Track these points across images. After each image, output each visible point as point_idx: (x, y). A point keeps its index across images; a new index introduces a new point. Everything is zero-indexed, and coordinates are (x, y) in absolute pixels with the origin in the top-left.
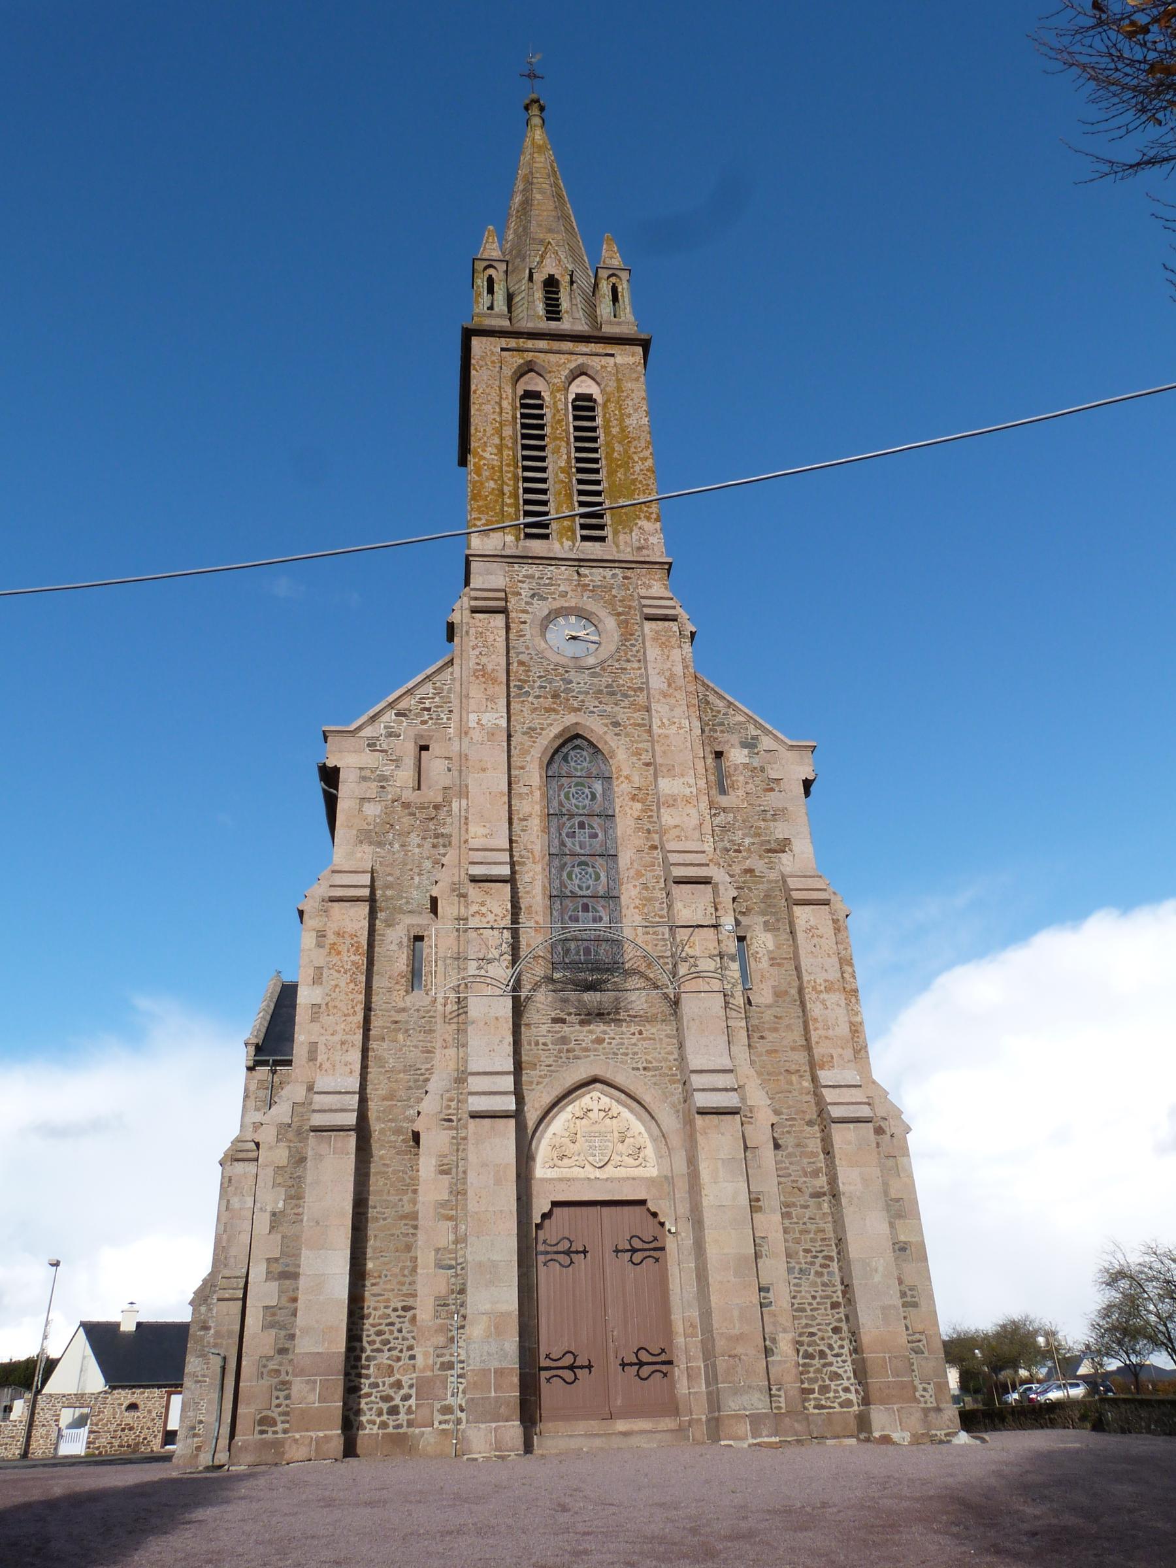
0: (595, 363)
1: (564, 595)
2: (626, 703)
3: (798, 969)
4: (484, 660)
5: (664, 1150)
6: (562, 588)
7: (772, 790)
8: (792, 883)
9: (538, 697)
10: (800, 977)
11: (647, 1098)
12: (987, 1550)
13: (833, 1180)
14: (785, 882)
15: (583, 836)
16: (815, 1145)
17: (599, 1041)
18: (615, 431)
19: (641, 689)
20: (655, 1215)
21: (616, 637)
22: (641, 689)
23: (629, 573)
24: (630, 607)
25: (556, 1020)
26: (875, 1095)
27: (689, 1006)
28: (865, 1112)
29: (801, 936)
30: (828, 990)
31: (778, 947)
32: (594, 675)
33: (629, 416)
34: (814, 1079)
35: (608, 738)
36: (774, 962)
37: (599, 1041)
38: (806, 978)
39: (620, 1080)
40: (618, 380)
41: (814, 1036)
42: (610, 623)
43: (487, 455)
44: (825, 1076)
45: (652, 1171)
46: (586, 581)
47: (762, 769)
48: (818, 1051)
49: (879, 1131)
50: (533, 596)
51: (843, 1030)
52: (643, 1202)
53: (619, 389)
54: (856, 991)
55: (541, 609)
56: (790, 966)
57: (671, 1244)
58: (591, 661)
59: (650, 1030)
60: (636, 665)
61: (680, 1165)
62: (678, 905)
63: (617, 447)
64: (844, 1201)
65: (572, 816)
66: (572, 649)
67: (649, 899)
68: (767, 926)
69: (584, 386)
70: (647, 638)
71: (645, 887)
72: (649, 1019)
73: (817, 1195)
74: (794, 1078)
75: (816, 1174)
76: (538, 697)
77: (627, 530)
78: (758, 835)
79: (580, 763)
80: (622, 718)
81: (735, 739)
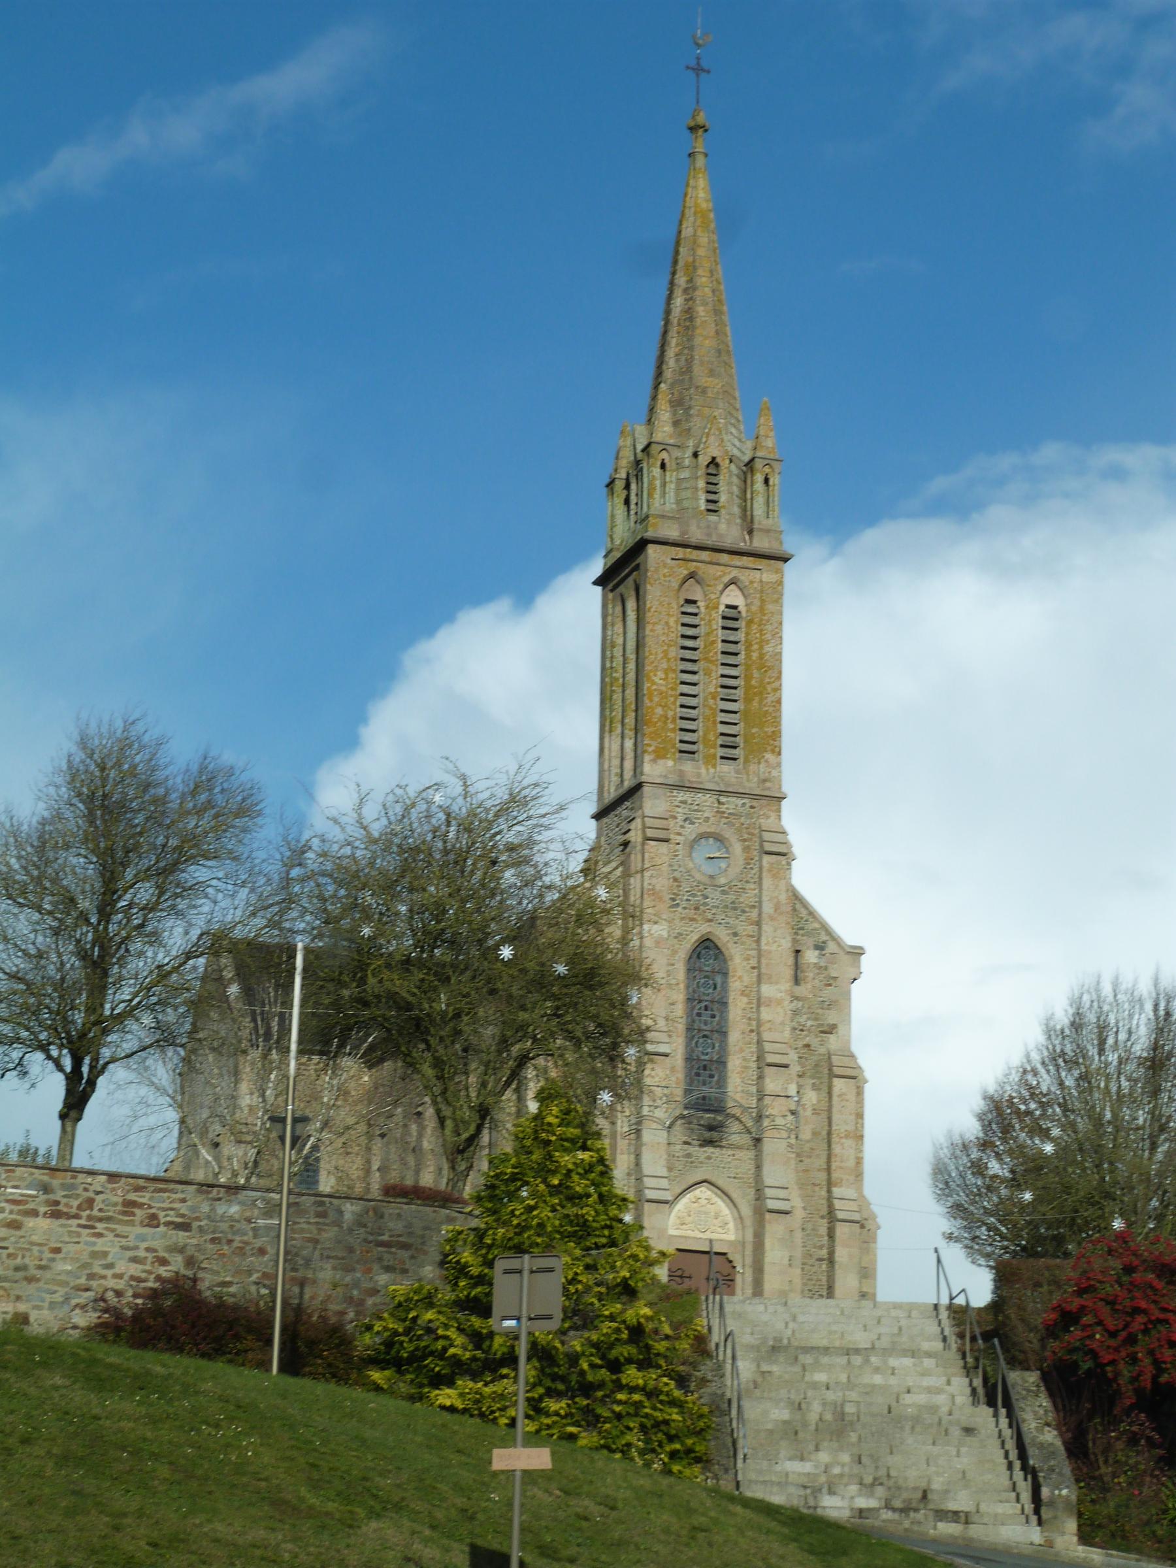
0: (744, 577)
1: (707, 819)
2: (742, 918)
3: (830, 1119)
4: (654, 881)
5: (740, 1226)
6: (706, 815)
7: (830, 985)
8: (836, 1060)
9: (685, 908)
10: (830, 1124)
11: (734, 1196)
12: (1078, 1014)
13: (831, 1253)
14: (829, 1058)
15: (706, 1017)
16: (823, 1231)
17: (709, 1158)
18: (755, 655)
19: (754, 907)
20: (731, 1262)
21: (741, 862)
22: (754, 907)
23: (755, 803)
24: (753, 834)
25: (686, 1143)
26: (862, 1202)
27: (768, 1146)
28: (856, 1217)
29: (835, 1099)
30: (847, 1137)
31: (819, 1101)
32: (724, 892)
33: (768, 642)
34: (829, 1191)
35: (729, 945)
36: (815, 1112)
37: (709, 1158)
38: (834, 1128)
39: (720, 1183)
40: (763, 601)
41: (834, 1165)
42: (737, 848)
43: (656, 679)
44: (837, 1191)
45: (731, 1236)
46: (723, 808)
47: (826, 968)
48: (835, 1175)
49: (862, 1226)
50: (685, 820)
51: (851, 1163)
52: (725, 1254)
53: (762, 609)
54: (862, 1136)
55: (690, 831)
56: (824, 1115)
57: (738, 1278)
58: (723, 881)
59: (740, 1154)
60: (752, 886)
61: (749, 1236)
62: (767, 1080)
63: (756, 674)
64: (837, 1266)
65: (700, 1001)
66: (708, 868)
67: (746, 1067)
68: (815, 1087)
69: (733, 597)
70: (764, 870)
71: (745, 1060)
72: (740, 1148)
73: (820, 1260)
74: (817, 1189)
75: (821, 1247)
76: (685, 908)
77: (756, 760)
78: (816, 1019)
79: (709, 964)
80: (740, 929)
81: (810, 942)
